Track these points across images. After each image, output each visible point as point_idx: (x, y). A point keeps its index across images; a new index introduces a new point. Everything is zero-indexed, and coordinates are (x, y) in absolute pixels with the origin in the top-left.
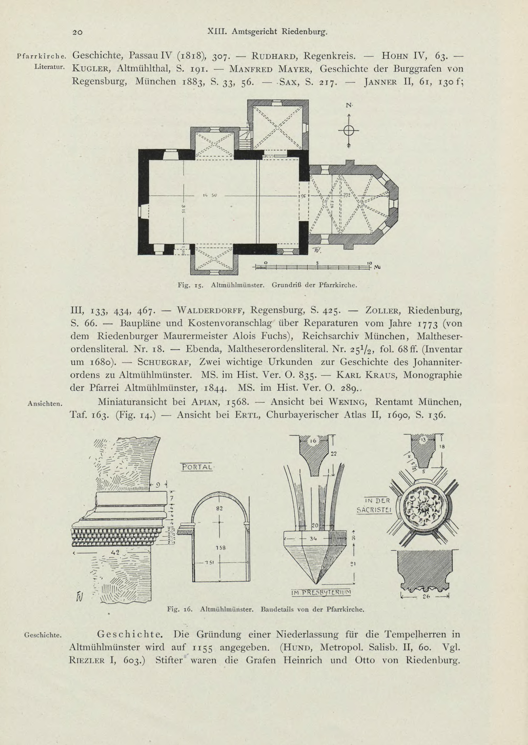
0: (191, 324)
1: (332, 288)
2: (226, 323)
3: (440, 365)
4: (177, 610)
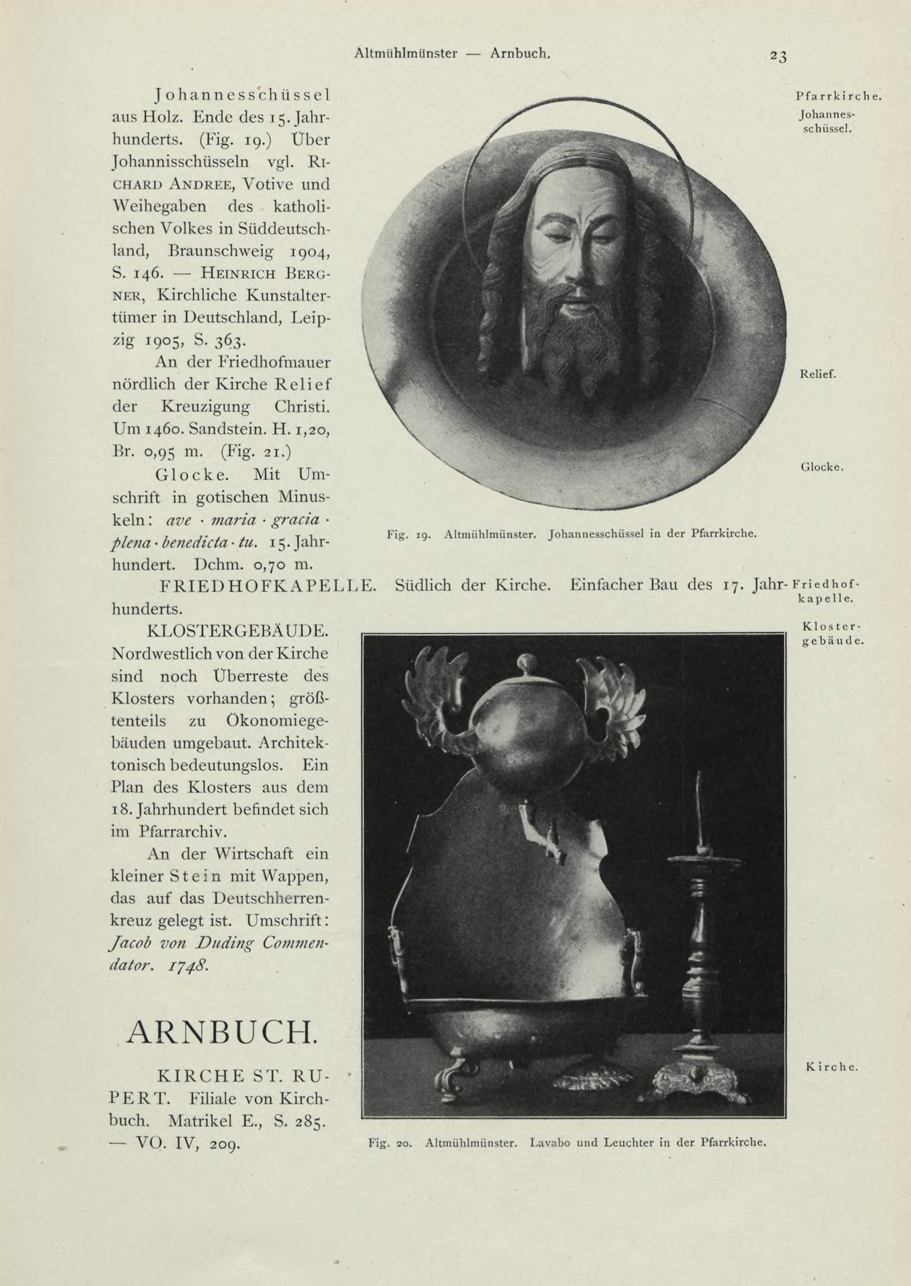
3: (141, 880)
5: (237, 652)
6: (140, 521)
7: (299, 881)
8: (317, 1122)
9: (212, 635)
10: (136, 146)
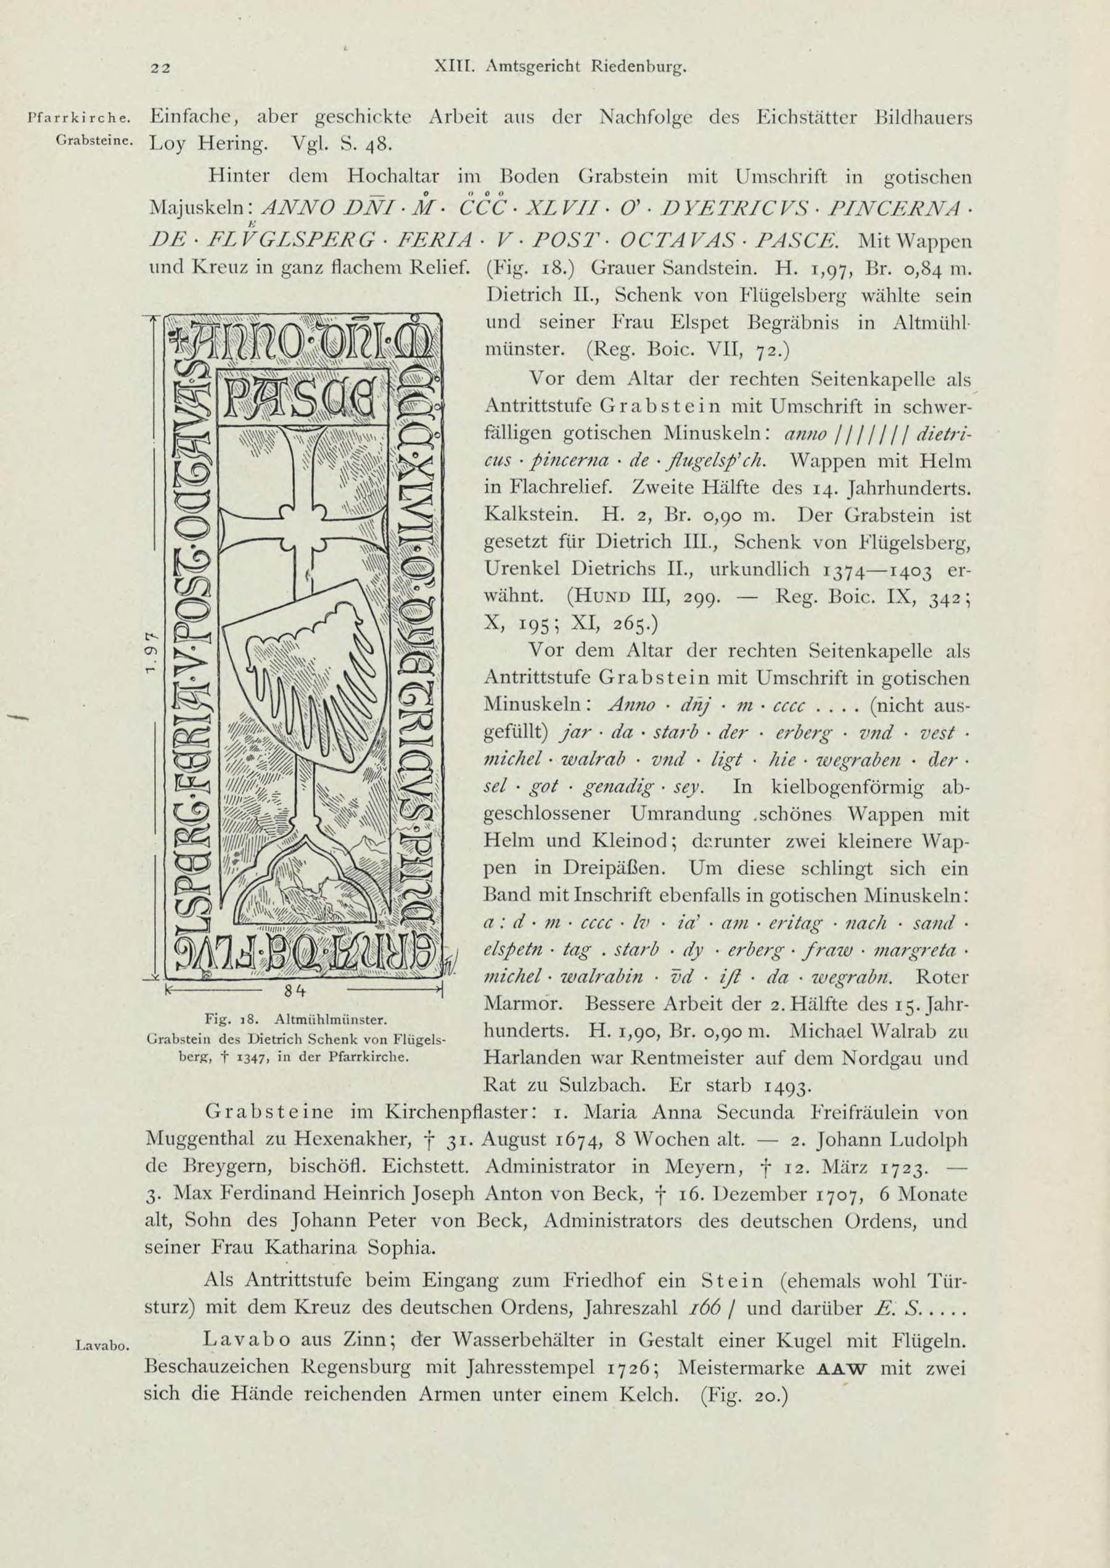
0: (625, 1396)
1: (356, 1063)
2: (871, 1223)
3: (511, 709)
4: (226, 1021)
6: (955, 897)
9: (673, 1090)
10: (533, 1012)
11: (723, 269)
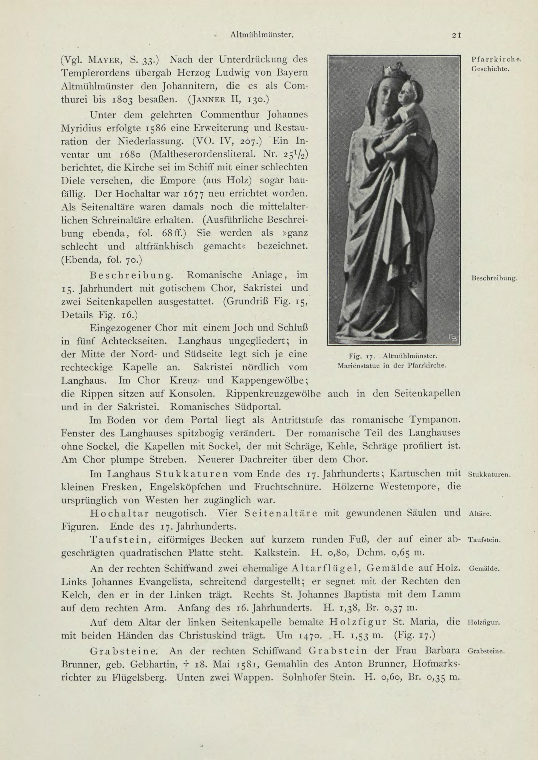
5: (185, 393)
7: (252, 383)
8: (408, 553)
11: (226, 553)
